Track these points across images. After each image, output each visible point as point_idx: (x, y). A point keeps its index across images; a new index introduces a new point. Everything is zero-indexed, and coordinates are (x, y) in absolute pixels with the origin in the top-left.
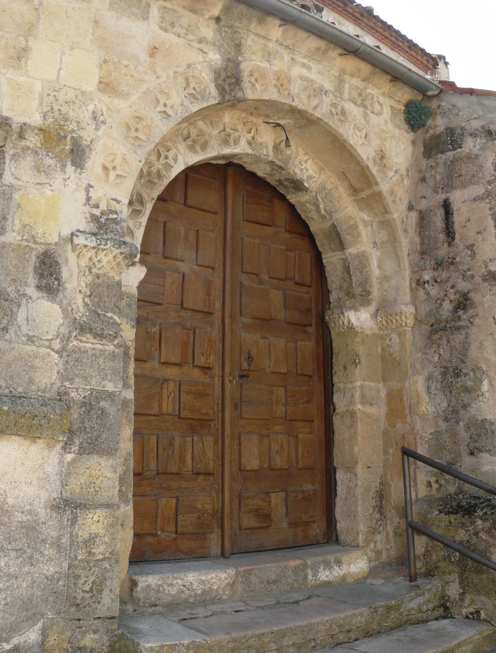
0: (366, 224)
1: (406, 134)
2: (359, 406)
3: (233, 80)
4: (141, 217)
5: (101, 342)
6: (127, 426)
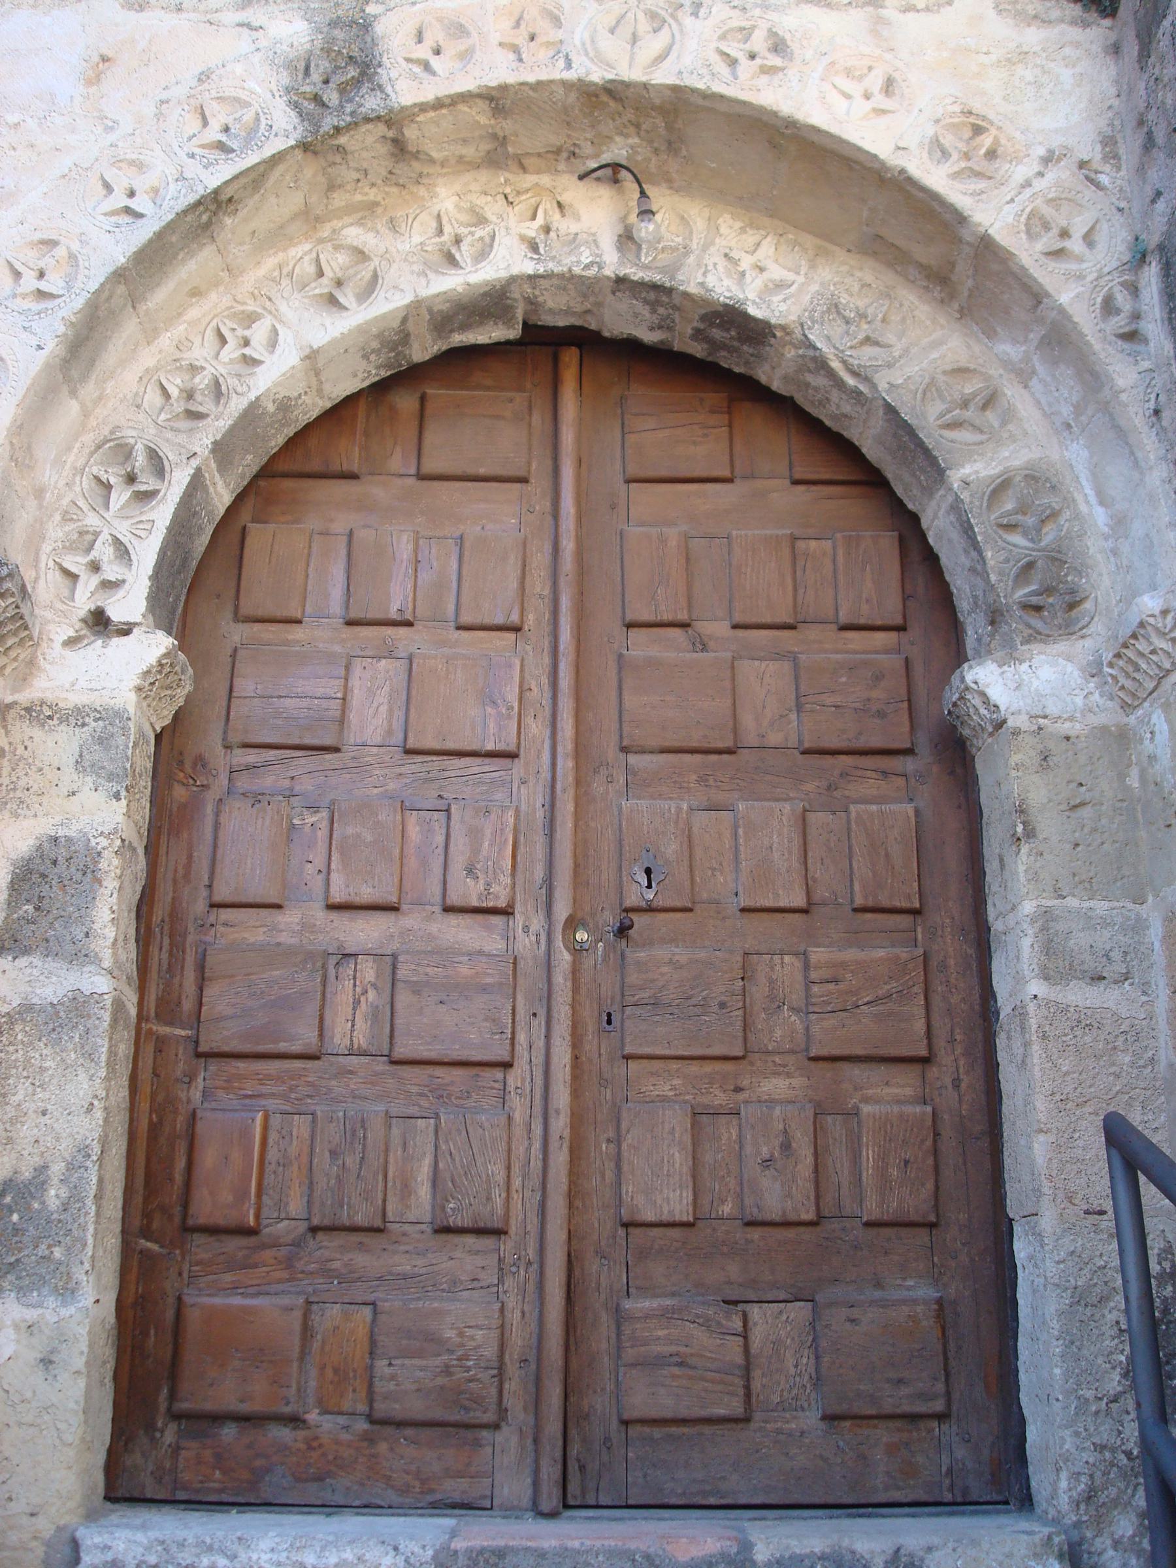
0: (1024, 376)
1: (1075, 33)
2: (1036, 987)
3: (353, 72)
4: (153, 508)
6: (80, 1070)
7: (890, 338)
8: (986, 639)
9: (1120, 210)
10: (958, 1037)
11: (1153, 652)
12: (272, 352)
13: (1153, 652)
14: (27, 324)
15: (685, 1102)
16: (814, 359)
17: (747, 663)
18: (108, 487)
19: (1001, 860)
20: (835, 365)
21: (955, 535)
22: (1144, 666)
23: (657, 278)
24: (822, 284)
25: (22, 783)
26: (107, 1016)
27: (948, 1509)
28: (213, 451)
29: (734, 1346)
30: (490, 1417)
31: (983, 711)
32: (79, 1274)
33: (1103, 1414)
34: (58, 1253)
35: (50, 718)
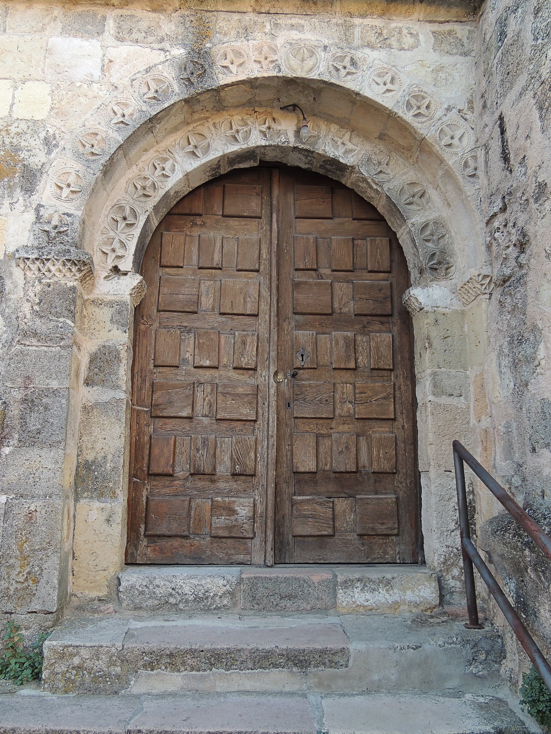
2: (431, 398)
5: (46, 345)
6: (116, 425)
7: (389, 171)
8: (418, 279)
9: (472, 129)
10: (404, 412)
11: (474, 288)
12: (173, 173)
13: (474, 288)
14: (89, 165)
15: (315, 433)
16: (362, 178)
17: (336, 283)
18: (117, 221)
19: (420, 354)
20: (369, 180)
21: (409, 241)
22: (471, 292)
23: (308, 147)
24: (366, 151)
25: (92, 327)
26: (125, 407)
27: (398, 565)
28: (154, 209)
29: (330, 511)
30: (251, 535)
31: (416, 304)
32: (118, 492)
33: (448, 536)
34: (111, 485)
35: (101, 304)
